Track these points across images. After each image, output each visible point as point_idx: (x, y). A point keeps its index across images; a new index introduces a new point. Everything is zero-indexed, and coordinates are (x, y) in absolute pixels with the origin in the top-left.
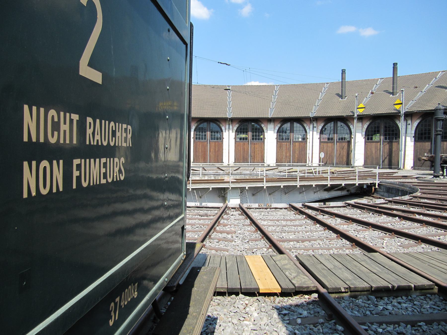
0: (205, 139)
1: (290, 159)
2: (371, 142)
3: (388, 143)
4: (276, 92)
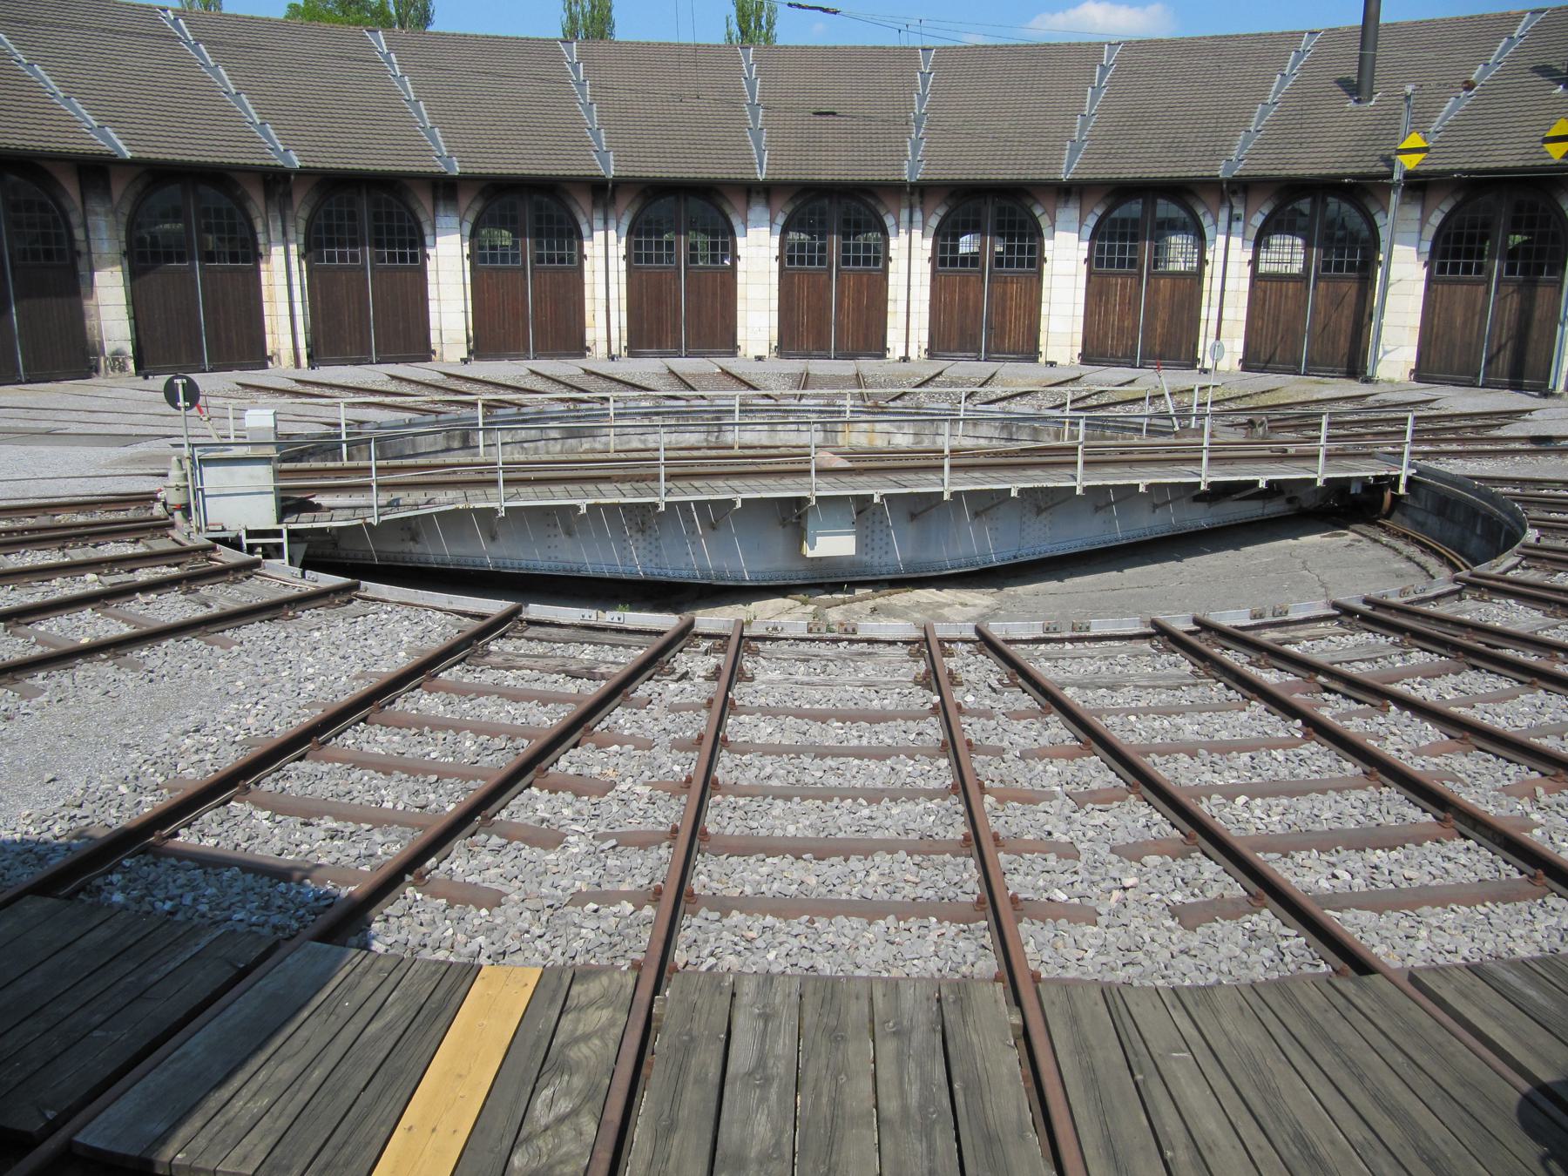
0: (821, 261)
1: (1135, 339)
2: (1450, 282)
3: (1520, 287)
4: (1104, 69)
